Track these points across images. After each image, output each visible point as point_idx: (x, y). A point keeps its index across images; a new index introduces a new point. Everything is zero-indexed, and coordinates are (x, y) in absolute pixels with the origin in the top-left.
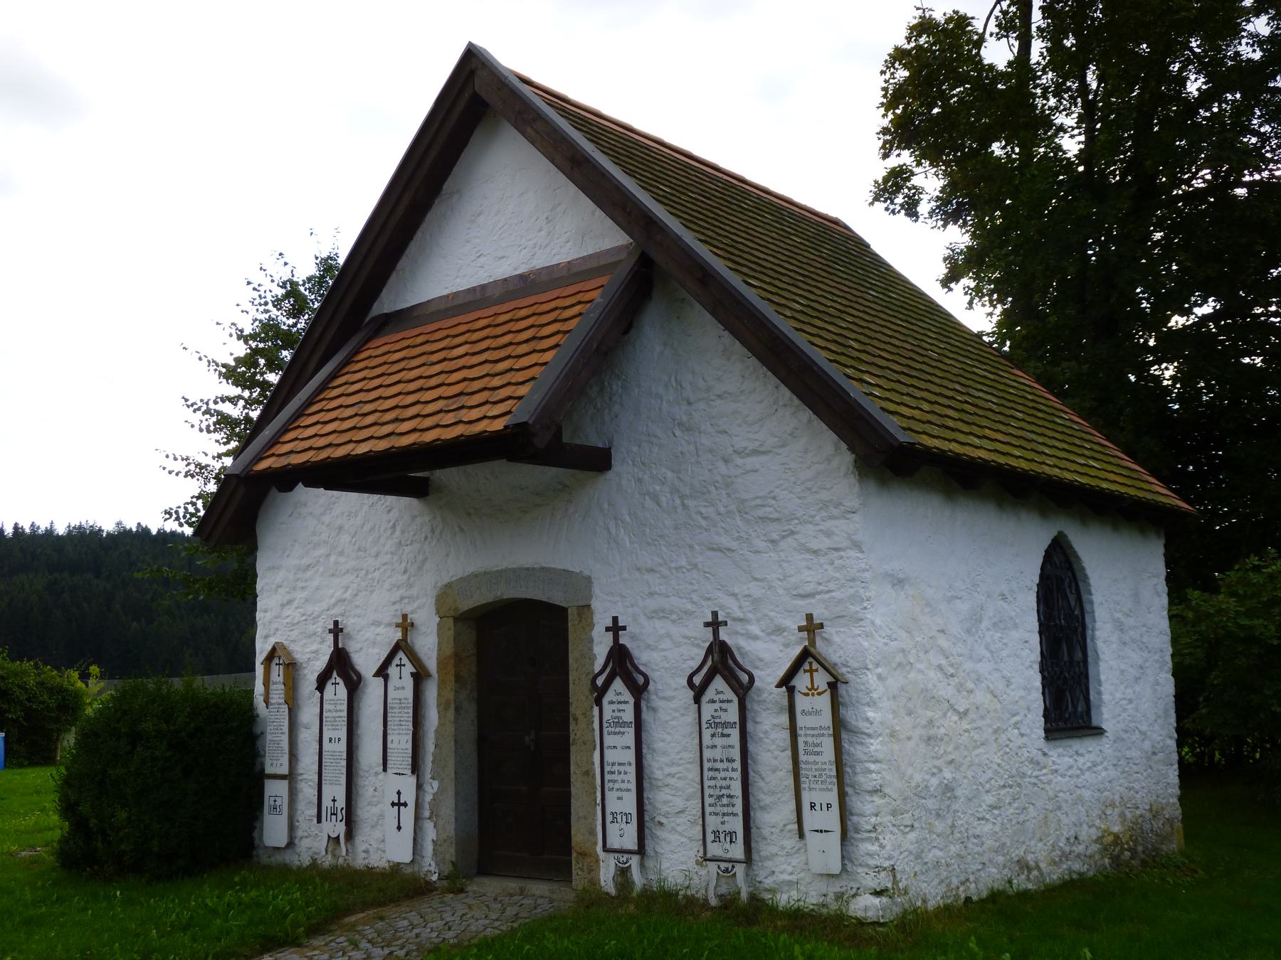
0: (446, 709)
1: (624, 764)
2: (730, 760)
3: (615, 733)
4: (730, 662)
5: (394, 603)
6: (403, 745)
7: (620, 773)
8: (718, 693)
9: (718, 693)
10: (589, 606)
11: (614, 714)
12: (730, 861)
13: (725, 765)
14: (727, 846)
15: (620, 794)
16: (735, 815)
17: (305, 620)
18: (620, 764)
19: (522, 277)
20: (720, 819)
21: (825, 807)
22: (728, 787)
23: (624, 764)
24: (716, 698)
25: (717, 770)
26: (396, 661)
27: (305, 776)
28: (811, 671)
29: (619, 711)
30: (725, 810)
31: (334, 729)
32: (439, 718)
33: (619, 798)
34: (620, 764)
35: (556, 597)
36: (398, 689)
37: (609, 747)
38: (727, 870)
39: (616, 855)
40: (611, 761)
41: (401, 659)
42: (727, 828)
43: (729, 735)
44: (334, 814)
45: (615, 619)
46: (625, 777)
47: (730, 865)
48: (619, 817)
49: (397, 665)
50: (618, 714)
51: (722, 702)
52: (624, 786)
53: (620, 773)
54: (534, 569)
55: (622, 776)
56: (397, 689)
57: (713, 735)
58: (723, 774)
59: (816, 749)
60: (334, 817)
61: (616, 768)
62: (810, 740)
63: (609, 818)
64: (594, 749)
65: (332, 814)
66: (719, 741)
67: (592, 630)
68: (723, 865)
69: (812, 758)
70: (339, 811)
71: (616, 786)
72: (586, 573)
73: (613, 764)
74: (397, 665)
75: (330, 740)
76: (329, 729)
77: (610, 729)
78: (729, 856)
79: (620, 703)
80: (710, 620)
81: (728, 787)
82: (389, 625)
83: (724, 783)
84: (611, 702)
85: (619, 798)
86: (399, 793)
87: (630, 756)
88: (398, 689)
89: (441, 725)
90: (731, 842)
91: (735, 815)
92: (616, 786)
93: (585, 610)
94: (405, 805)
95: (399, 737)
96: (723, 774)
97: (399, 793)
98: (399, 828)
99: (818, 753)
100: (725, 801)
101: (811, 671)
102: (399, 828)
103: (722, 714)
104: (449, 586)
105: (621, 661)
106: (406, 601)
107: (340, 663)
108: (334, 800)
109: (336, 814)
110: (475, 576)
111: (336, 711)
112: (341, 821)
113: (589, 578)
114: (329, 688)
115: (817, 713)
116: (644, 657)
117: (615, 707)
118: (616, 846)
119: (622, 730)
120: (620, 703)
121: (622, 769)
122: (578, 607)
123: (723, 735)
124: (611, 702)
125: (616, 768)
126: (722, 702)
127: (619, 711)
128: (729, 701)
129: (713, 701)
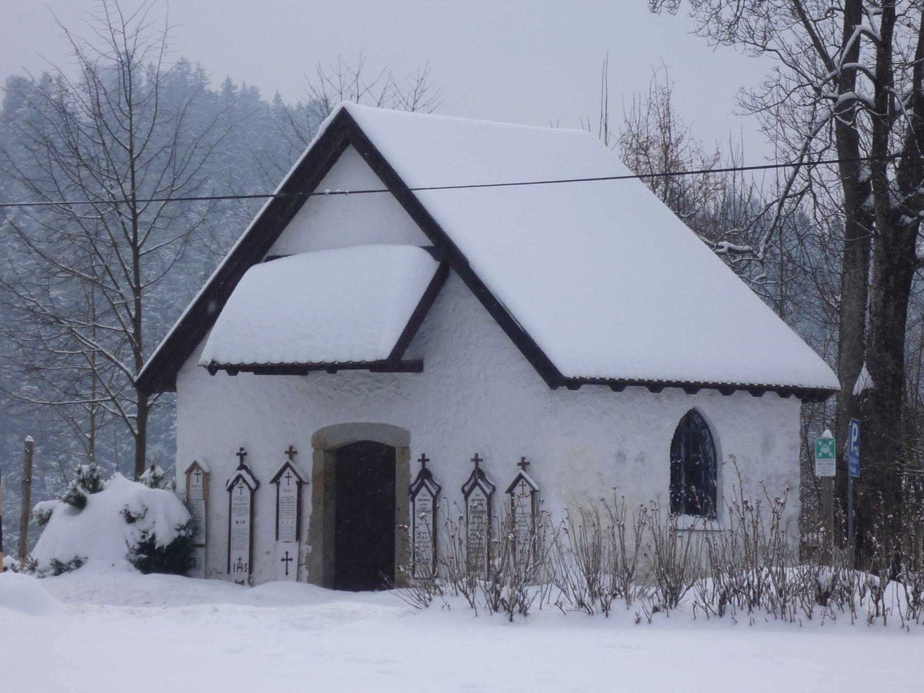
8: (477, 495)
9: (477, 495)
24: (476, 498)
26: (285, 474)
29: (424, 504)
35: (388, 440)
36: (287, 491)
41: (288, 473)
50: (424, 506)
56: (285, 491)
60: (240, 570)
74: (286, 477)
75: (237, 522)
79: (425, 500)
84: (420, 500)
86: (287, 553)
93: (406, 450)
94: (291, 560)
97: (287, 553)
101: (523, 486)
104: (322, 430)
120: (425, 500)
124: (420, 500)
127: (424, 504)
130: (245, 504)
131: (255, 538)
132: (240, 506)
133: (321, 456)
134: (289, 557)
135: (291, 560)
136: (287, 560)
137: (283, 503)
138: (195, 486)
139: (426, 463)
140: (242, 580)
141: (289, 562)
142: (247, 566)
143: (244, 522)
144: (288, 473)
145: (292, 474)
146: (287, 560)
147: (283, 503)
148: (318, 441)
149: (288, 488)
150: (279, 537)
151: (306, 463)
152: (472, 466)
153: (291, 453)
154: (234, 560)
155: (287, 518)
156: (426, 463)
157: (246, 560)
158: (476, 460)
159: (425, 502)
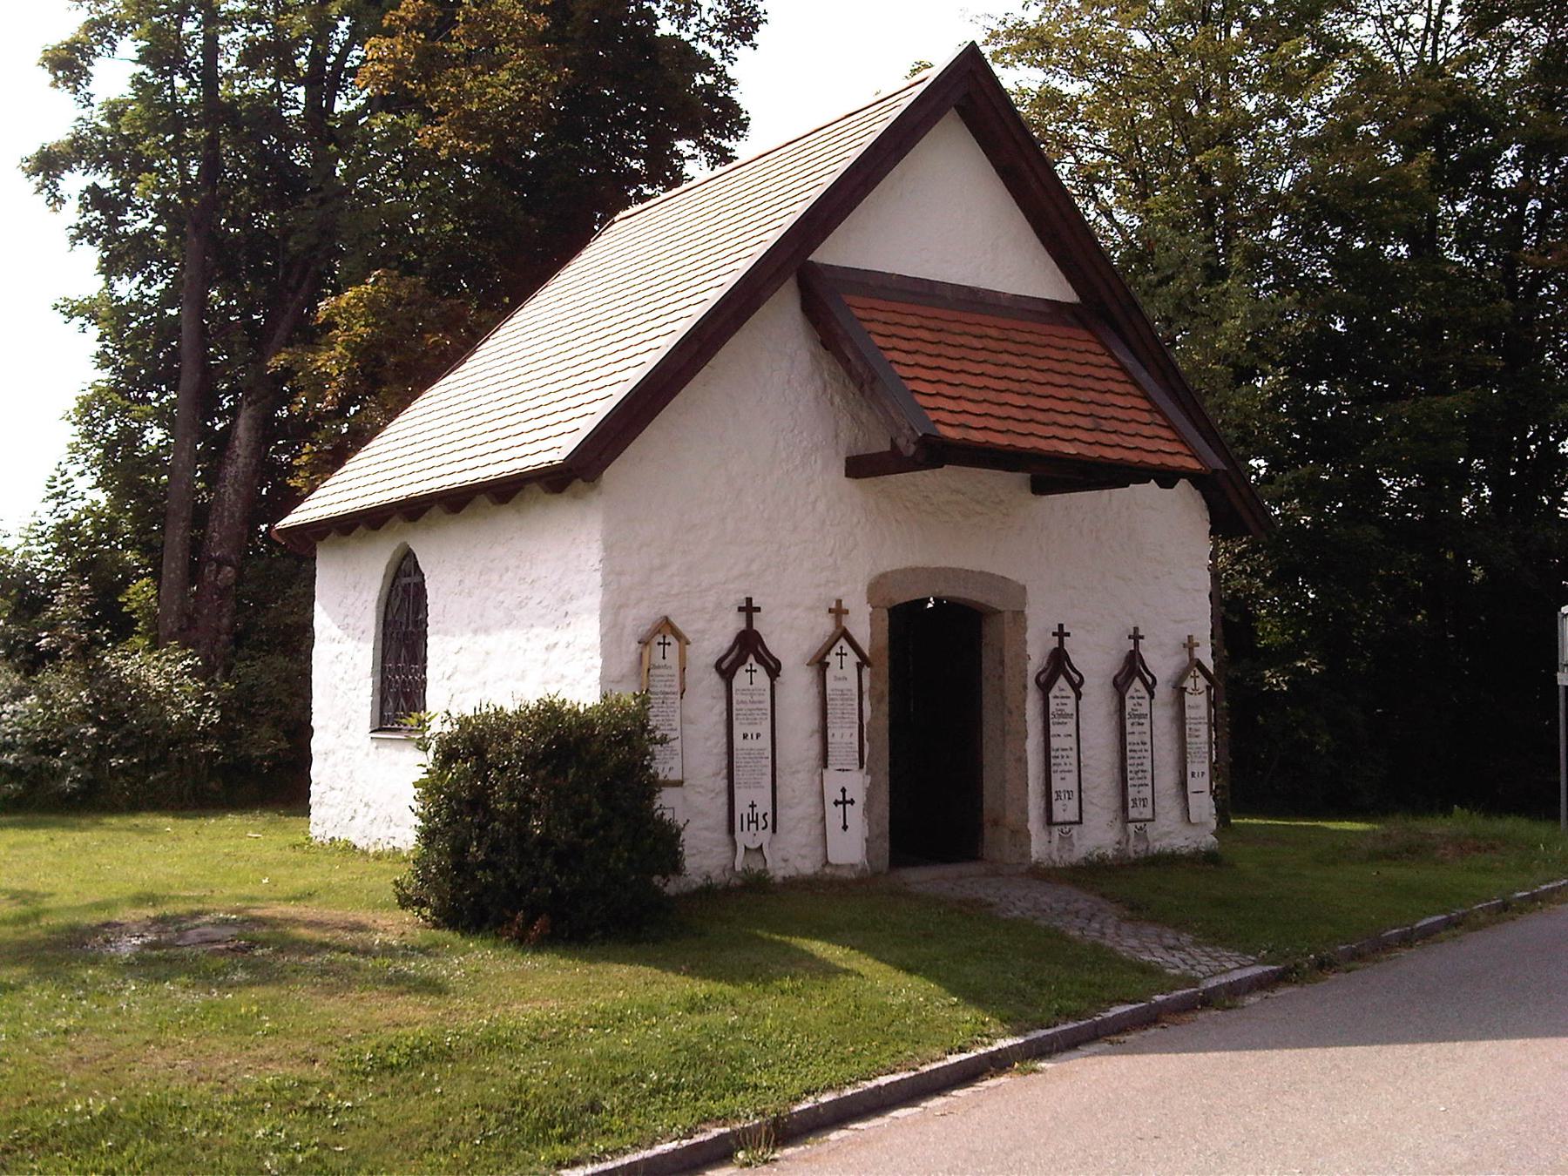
0: (879, 701)
1: (1066, 750)
2: (1144, 743)
3: (1059, 723)
4: (760, 649)
5: (819, 586)
6: (847, 739)
7: (1063, 757)
8: (1137, 691)
9: (1137, 691)
10: (1023, 612)
11: (1058, 708)
12: (1141, 821)
13: (1141, 747)
14: (1141, 809)
15: (1063, 775)
16: (1147, 785)
17: (688, 592)
18: (1063, 750)
19: (972, 291)
20: (1136, 788)
21: (755, 737)
22: (1142, 764)
23: (1066, 750)
24: (1135, 695)
25: (1135, 751)
26: (836, 649)
27: (692, 782)
28: (1195, 677)
29: (1063, 704)
30: (1140, 782)
31: (750, 724)
32: (872, 711)
33: (1063, 779)
34: (1063, 750)
35: (995, 601)
36: (840, 679)
37: (1054, 736)
38: (1141, 828)
39: (1060, 827)
40: (1055, 747)
41: (841, 648)
42: (1141, 796)
43: (1142, 724)
44: (753, 821)
45: (1136, 629)
46: (1067, 761)
47: (1142, 824)
48: (1062, 795)
49: (837, 654)
50: (1062, 707)
51: (1139, 698)
52: (1066, 768)
53: (1063, 757)
54: (972, 571)
55: (1065, 760)
56: (837, 679)
57: (1132, 724)
58: (1139, 754)
59: (1197, 734)
60: (753, 826)
61: (1060, 753)
62: (1192, 726)
63: (1054, 796)
64: (869, 724)
65: (749, 822)
66: (1137, 729)
67: (1025, 633)
68: (1138, 825)
69: (1194, 740)
70: (760, 818)
71: (1060, 768)
72: (1022, 582)
73: (1058, 750)
74: (837, 654)
75: (745, 736)
76: (741, 724)
77: (1056, 720)
78: (1143, 817)
79: (1063, 697)
80: (1132, 634)
81: (1142, 764)
82: (811, 609)
83: (1139, 761)
84: (1056, 697)
85: (1063, 779)
86: (843, 790)
87: (1072, 742)
88: (840, 679)
89: (873, 718)
90: (1144, 806)
91: (1147, 785)
92: (1060, 768)
93: (1019, 616)
94: (836, 803)
95: (841, 731)
96: (1139, 754)
97: (843, 790)
98: (845, 827)
99: (1197, 736)
100: (1140, 775)
101: (1195, 677)
102: (845, 827)
103: (1138, 707)
104: (884, 576)
105: (1059, 662)
106: (831, 585)
107: (749, 645)
108: (753, 806)
109: (757, 822)
110: (914, 570)
111: (753, 702)
112: (764, 829)
113: (1024, 588)
114: (741, 679)
115: (1197, 707)
116: (773, 645)
117: (1058, 701)
118: (1060, 820)
119: (1065, 720)
120: (1063, 697)
121: (1064, 753)
122: (1013, 612)
123: (1139, 724)
124: (1056, 697)
125: (1060, 753)
126: (1139, 698)
127: (1063, 704)
128: (1143, 698)
129: (1133, 698)
130: (760, 702)
131: (1114, 723)
132: (750, 706)
133: (883, 620)
134: (847, 798)
135: (836, 803)
136: (844, 802)
137: (832, 699)
138: (659, 667)
139: (1065, 638)
140: (757, 845)
141: (848, 806)
142: (769, 818)
143: (758, 735)
144: (841, 648)
145: (847, 648)
146: (844, 802)
147: (832, 699)
148: (876, 588)
149: (840, 673)
150: (831, 759)
151: (861, 626)
152: (736, 623)
153: (838, 612)
154: (741, 808)
155: (842, 727)
156: (755, 615)
157: (764, 806)
158: (749, 609)
159: (1064, 701)
